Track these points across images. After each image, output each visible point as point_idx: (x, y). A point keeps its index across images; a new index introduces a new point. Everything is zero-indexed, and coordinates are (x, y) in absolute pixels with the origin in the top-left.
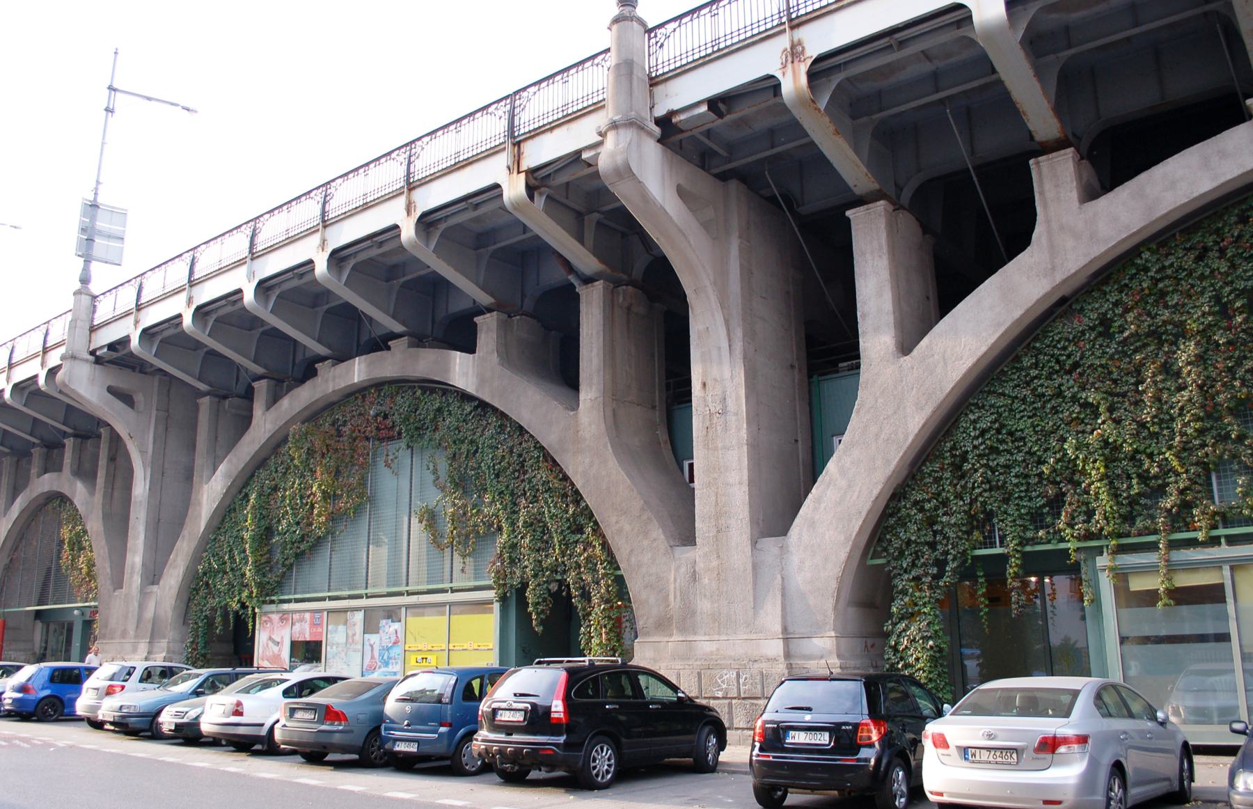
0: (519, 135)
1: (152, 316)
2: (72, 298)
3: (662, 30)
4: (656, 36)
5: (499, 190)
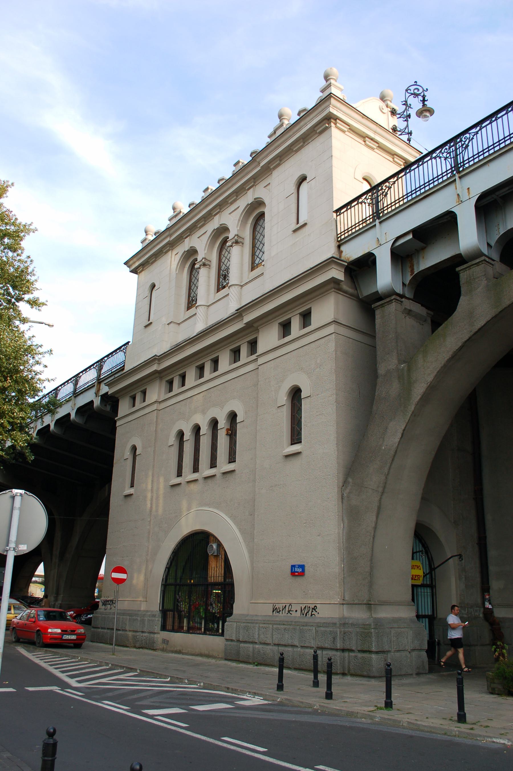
1: (82, 401)
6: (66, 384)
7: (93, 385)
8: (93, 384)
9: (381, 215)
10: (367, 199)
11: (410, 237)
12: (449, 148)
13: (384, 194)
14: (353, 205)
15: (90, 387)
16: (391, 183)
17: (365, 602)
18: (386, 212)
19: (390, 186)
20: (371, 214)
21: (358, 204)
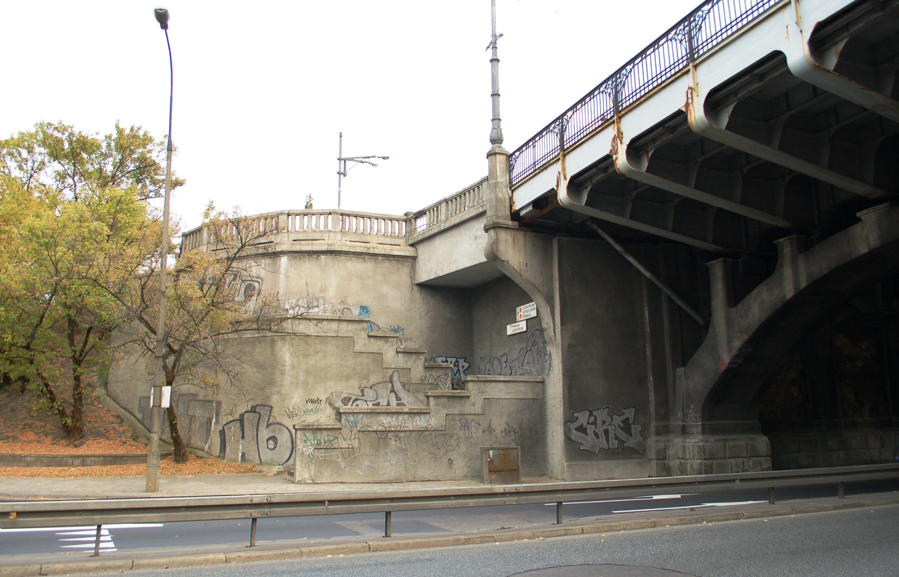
0: (622, 110)
1: (579, 161)
2: (486, 162)
3: (700, 13)
4: (620, 77)
5: (780, 58)
6: (524, 148)
7: (611, 121)
8: (556, 157)
9: (696, 56)
10: (678, 35)
11: (530, 208)
12: (684, 29)
13: (698, 27)
14: (661, 43)
15: (571, 148)
16: (705, 12)
17: (211, 457)
18: (701, 52)
19: (704, 16)
20: (684, 54)
21: (667, 41)
